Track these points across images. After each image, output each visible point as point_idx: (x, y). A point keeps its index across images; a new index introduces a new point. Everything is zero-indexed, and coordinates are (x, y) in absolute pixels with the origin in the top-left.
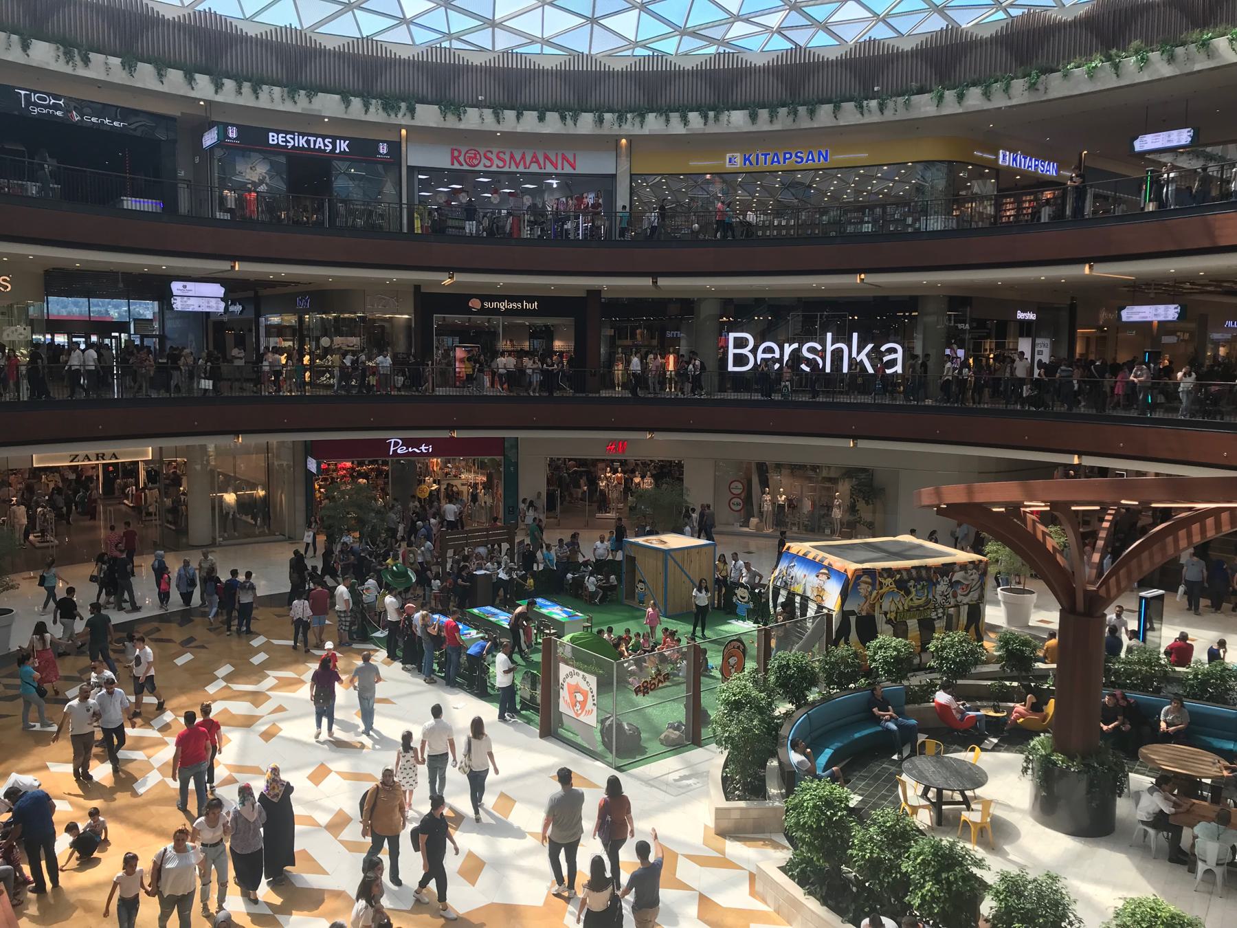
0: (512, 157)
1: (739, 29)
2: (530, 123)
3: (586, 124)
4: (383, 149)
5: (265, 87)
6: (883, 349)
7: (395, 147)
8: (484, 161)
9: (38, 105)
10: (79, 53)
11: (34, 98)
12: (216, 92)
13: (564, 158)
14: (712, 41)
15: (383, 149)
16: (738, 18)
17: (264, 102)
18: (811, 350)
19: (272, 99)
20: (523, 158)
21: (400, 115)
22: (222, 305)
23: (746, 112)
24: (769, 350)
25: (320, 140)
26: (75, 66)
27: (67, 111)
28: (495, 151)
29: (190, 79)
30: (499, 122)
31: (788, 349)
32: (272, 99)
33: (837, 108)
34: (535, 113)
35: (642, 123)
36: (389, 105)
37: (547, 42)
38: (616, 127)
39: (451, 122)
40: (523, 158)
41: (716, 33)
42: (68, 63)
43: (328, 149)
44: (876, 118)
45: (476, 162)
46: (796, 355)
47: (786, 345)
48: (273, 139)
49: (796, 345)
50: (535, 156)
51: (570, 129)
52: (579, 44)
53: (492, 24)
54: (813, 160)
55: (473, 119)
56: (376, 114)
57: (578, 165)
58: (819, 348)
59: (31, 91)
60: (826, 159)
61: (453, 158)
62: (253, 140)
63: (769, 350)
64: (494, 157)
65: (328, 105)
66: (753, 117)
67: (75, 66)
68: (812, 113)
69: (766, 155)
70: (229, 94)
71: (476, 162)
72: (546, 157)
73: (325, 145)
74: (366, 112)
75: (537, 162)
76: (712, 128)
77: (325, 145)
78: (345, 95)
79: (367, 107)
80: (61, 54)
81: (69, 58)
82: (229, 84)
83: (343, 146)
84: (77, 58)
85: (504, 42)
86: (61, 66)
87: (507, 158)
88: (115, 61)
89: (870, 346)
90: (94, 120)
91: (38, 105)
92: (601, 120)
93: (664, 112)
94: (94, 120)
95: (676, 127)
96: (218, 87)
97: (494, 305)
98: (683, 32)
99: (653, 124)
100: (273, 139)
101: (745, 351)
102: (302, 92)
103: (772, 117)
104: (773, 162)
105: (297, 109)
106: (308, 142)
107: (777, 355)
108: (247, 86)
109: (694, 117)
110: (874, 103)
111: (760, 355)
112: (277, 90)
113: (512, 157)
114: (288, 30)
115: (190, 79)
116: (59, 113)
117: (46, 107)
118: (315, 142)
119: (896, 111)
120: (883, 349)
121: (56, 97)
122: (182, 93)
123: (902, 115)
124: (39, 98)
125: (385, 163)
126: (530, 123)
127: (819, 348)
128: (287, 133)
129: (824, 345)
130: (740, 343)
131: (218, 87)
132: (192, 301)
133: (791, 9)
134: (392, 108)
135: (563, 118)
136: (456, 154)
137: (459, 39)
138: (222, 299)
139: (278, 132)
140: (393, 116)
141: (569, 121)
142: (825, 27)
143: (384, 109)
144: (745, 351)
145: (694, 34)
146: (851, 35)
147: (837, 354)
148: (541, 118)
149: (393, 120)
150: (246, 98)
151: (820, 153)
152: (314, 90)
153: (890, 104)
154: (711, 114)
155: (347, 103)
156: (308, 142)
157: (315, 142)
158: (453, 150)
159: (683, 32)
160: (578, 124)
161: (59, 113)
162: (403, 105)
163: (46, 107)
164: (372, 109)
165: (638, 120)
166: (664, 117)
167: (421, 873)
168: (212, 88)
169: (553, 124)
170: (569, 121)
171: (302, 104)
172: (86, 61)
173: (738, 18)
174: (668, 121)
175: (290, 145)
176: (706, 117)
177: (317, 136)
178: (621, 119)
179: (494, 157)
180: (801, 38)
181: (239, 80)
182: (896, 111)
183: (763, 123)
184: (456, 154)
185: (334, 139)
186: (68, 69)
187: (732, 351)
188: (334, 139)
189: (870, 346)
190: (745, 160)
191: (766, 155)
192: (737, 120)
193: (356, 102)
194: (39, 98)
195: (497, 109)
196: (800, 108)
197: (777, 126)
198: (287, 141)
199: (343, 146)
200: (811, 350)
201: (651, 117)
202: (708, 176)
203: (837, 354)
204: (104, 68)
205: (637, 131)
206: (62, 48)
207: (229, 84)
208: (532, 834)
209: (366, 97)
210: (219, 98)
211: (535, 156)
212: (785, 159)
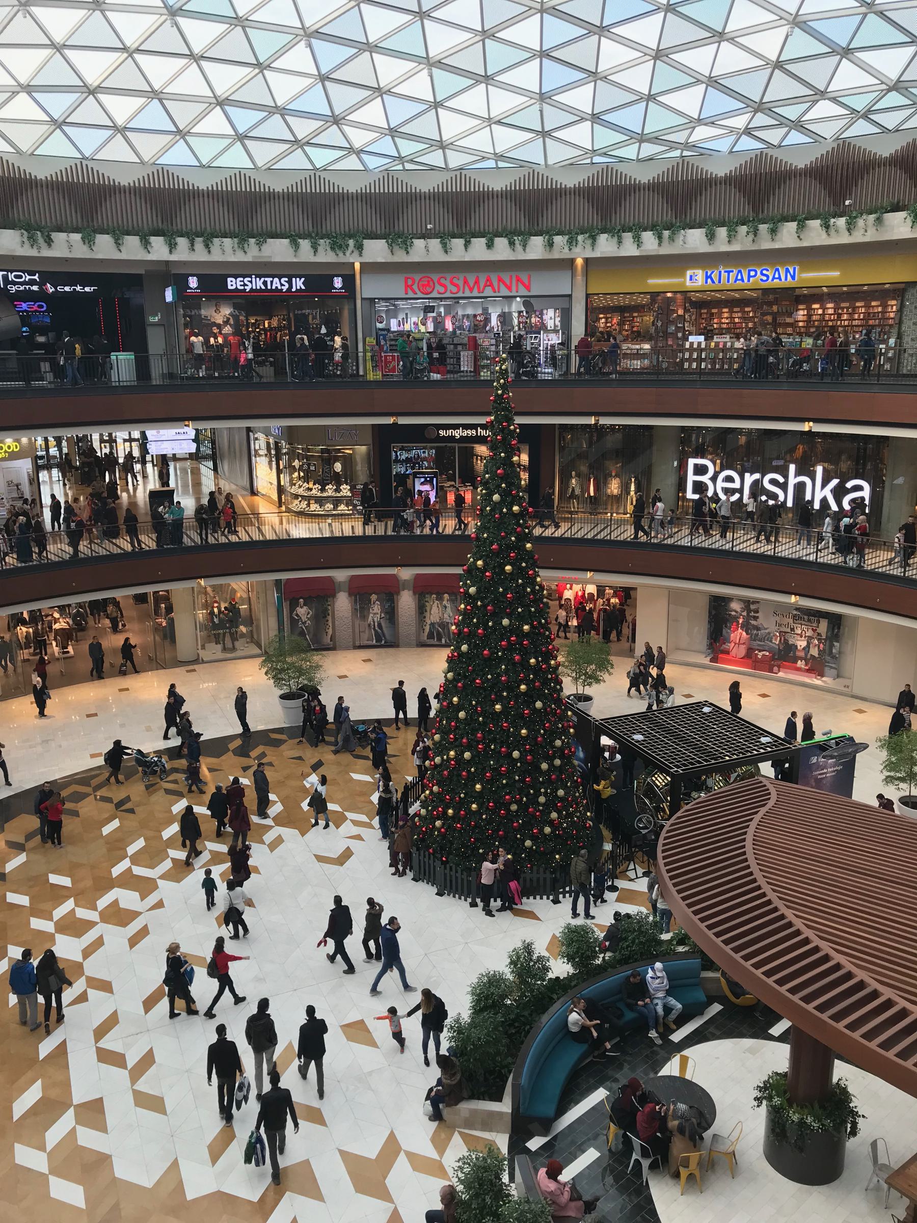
0: (466, 282)
1: (701, 133)
2: (478, 250)
3: (536, 248)
4: (338, 283)
5: (216, 240)
6: (849, 485)
7: (349, 280)
8: (438, 288)
9: (15, 283)
10: (42, 234)
11: (11, 277)
12: (171, 252)
13: (518, 279)
14: (673, 146)
15: (338, 283)
16: (700, 121)
17: (216, 255)
18: (773, 482)
19: (225, 251)
20: (477, 282)
21: (348, 253)
22: (195, 445)
23: (704, 230)
24: (729, 479)
25: (276, 280)
26: (39, 248)
27: (41, 284)
28: (449, 276)
29: (146, 244)
30: (446, 252)
31: (749, 479)
32: (225, 251)
33: (801, 227)
34: (483, 241)
35: (593, 245)
36: (337, 246)
37: (499, 157)
38: (566, 250)
39: (400, 257)
40: (477, 282)
41: (680, 137)
42: (32, 246)
43: (285, 289)
44: (844, 239)
45: (429, 289)
46: (756, 484)
47: (747, 475)
48: (233, 284)
49: (757, 476)
50: (488, 279)
51: (520, 255)
52: (533, 154)
53: (442, 145)
54: (780, 278)
55: (425, 250)
56: (326, 256)
57: (533, 287)
58: (781, 480)
59: (7, 271)
60: (793, 277)
61: (407, 286)
62: (214, 284)
63: (729, 479)
64: (447, 283)
65: (278, 250)
66: (711, 237)
67: (39, 248)
68: (773, 231)
69: (729, 272)
70: (184, 252)
71: (429, 289)
72: (500, 280)
73: (282, 285)
74: (316, 251)
75: (491, 285)
76: (667, 249)
77: (282, 285)
78: (294, 239)
79: (315, 248)
80: (25, 239)
81: (33, 241)
82: (182, 242)
83: (299, 284)
84: (41, 240)
85: (456, 160)
86: (28, 251)
87: (460, 283)
88: (76, 237)
89: (835, 482)
90: (67, 289)
91: (15, 283)
92: (550, 244)
93: (616, 232)
94: (67, 289)
95: (629, 249)
96: (172, 246)
97: (449, 432)
98: (642, 138)
99: (606, 246)
100: (233, 284)
101: (705, 479)
102: (252, 241)
103: (729, 236)
104: (736, 280)
105: (248, 258)
106: (265, 283)
107: (737, 485)
108: (199, 241)
109: (648, 237)
110: (841, 222)
111: (720, 484)
112: (227, 242)
113: (466, 282)
114: (240, 174)
115: (146, 244)
116: (35, 288)
117: (22, 284)
118: (272, 282)
119: (866, 231)
120: (849, 485)
121: (32, 273)
122: (139, 257)
123: (871, 236)
124: (16, 277)
125: (338, 297)
126: (478, 250)
127: (781, 480)
128: (244, 276)
129: (786, 477)
130: (700, 470)
131: (172, 246)
132: (166, 444)
133: (756, 111)
134: (340, 247)
135: (512, 244)
136: (410, 282)
137: (412, 161)
138: (193, 441)
139: (236, 277)
140: (341, 254)
141: (519, 247)
142: (798, 125)
143: (332, 249)
144: (705, 479)
145: (655, 139)
146: (828, 131)
147: (800, 487)
148: (490, 245)
149: (342, 259)
150: (200, 255)
151: (787, 271)
152: (264, 236)
153: (860, 222)
154: (666, 233)
155: (296, 246)
156: (265, 283)
157: (272, 282)
158: (406, 279)
159: (642, 138)
160: (528, 249)
161: (35, 288)
162: (351, 242)
163: (22, 284)
164: (320, 249)
165: (589, 242)
166: (616, 239)
167: (628, 686)
168: (166, 249)
169: (502, 250)
170: (519, 247)
171: (252, 253)
172: (49, 242)
173: (700, 121)
174: (620, 242)
175: (248, 289)
176: (660, 238)
177: (273, 276)
178: (572, 242)
179: (447, 283)
180: (774, 136)
181: (191, 236)
182: (866, 231)
183: (722, 244)
184: (410, 282)
185: (290, 278)
186: (33, 253)
187: (691, 478)
188: (290, 278)
189: (835, 482)
190: (707, 277)
191: (729, 272)
192: (694, 240)
193: (305, 244)
194: (16, 277)
195: (444, 237)
196: (761, 227)
197: (736, 247)
198: (245, 285)
199: (299, 284)
200: (773, 482)
201: (603, 238)
202: (669, 295)
203: (800, 487)
204: (67, 246)
205: (590, 254)
206: (25, 233)
207: (182, 242)
208: (403, 1017)
209: (314, 237)
210: (174, 258)
211: (488, 279)
212: (749, 277)
